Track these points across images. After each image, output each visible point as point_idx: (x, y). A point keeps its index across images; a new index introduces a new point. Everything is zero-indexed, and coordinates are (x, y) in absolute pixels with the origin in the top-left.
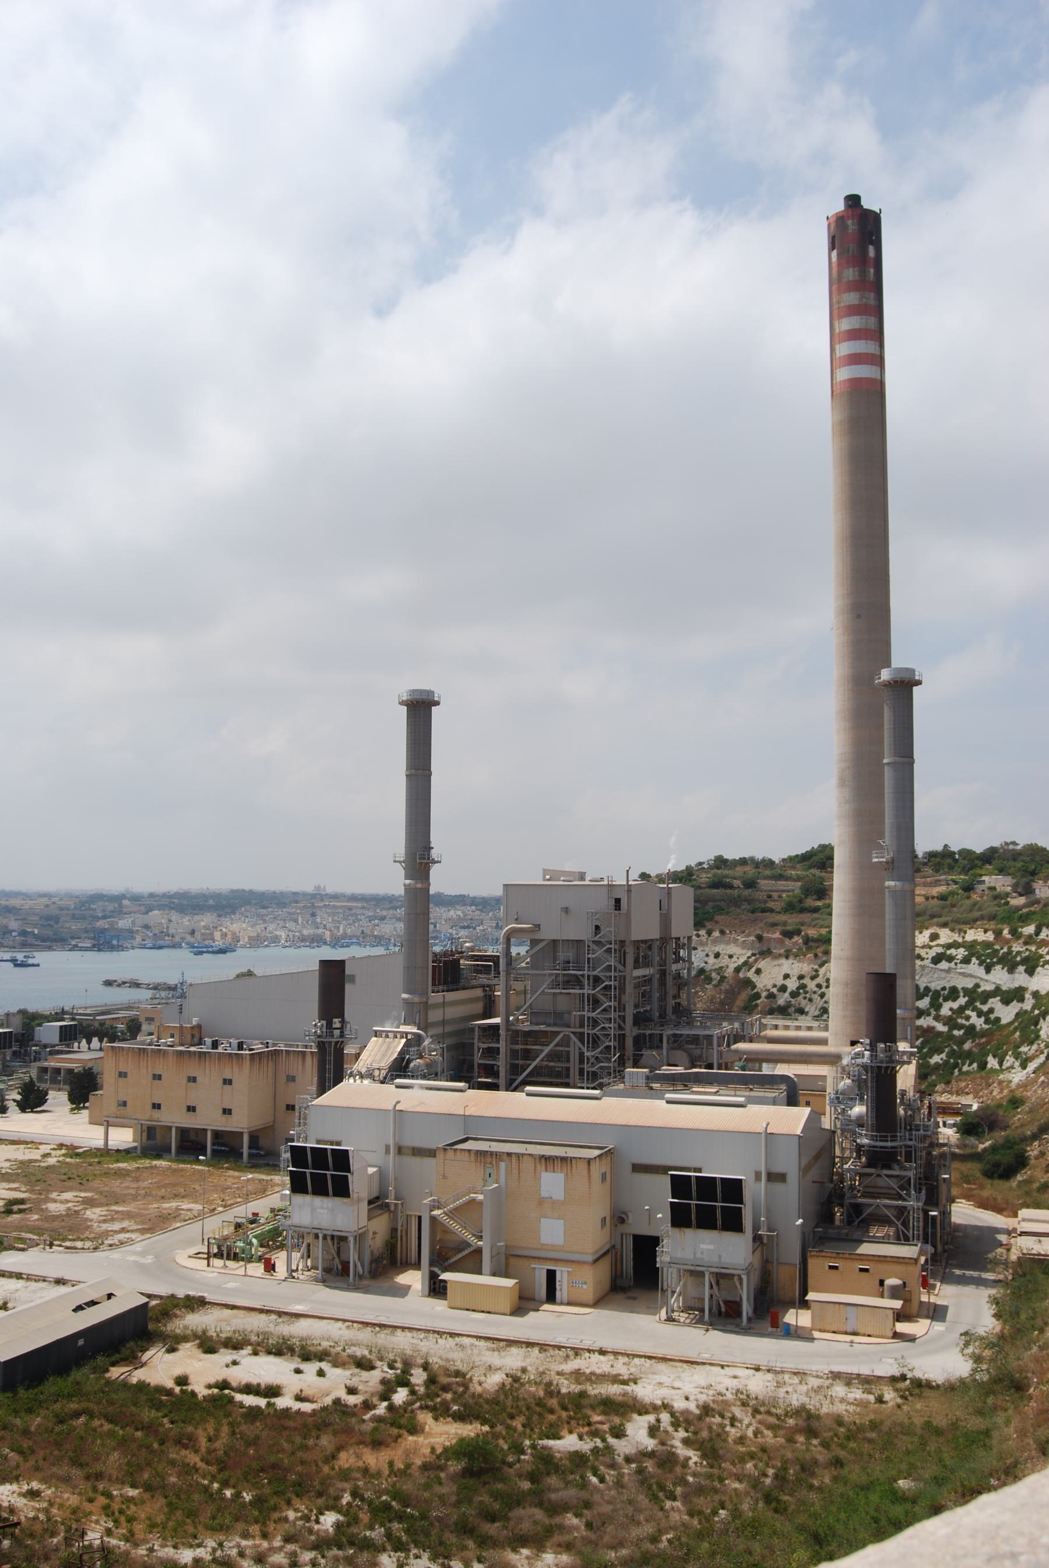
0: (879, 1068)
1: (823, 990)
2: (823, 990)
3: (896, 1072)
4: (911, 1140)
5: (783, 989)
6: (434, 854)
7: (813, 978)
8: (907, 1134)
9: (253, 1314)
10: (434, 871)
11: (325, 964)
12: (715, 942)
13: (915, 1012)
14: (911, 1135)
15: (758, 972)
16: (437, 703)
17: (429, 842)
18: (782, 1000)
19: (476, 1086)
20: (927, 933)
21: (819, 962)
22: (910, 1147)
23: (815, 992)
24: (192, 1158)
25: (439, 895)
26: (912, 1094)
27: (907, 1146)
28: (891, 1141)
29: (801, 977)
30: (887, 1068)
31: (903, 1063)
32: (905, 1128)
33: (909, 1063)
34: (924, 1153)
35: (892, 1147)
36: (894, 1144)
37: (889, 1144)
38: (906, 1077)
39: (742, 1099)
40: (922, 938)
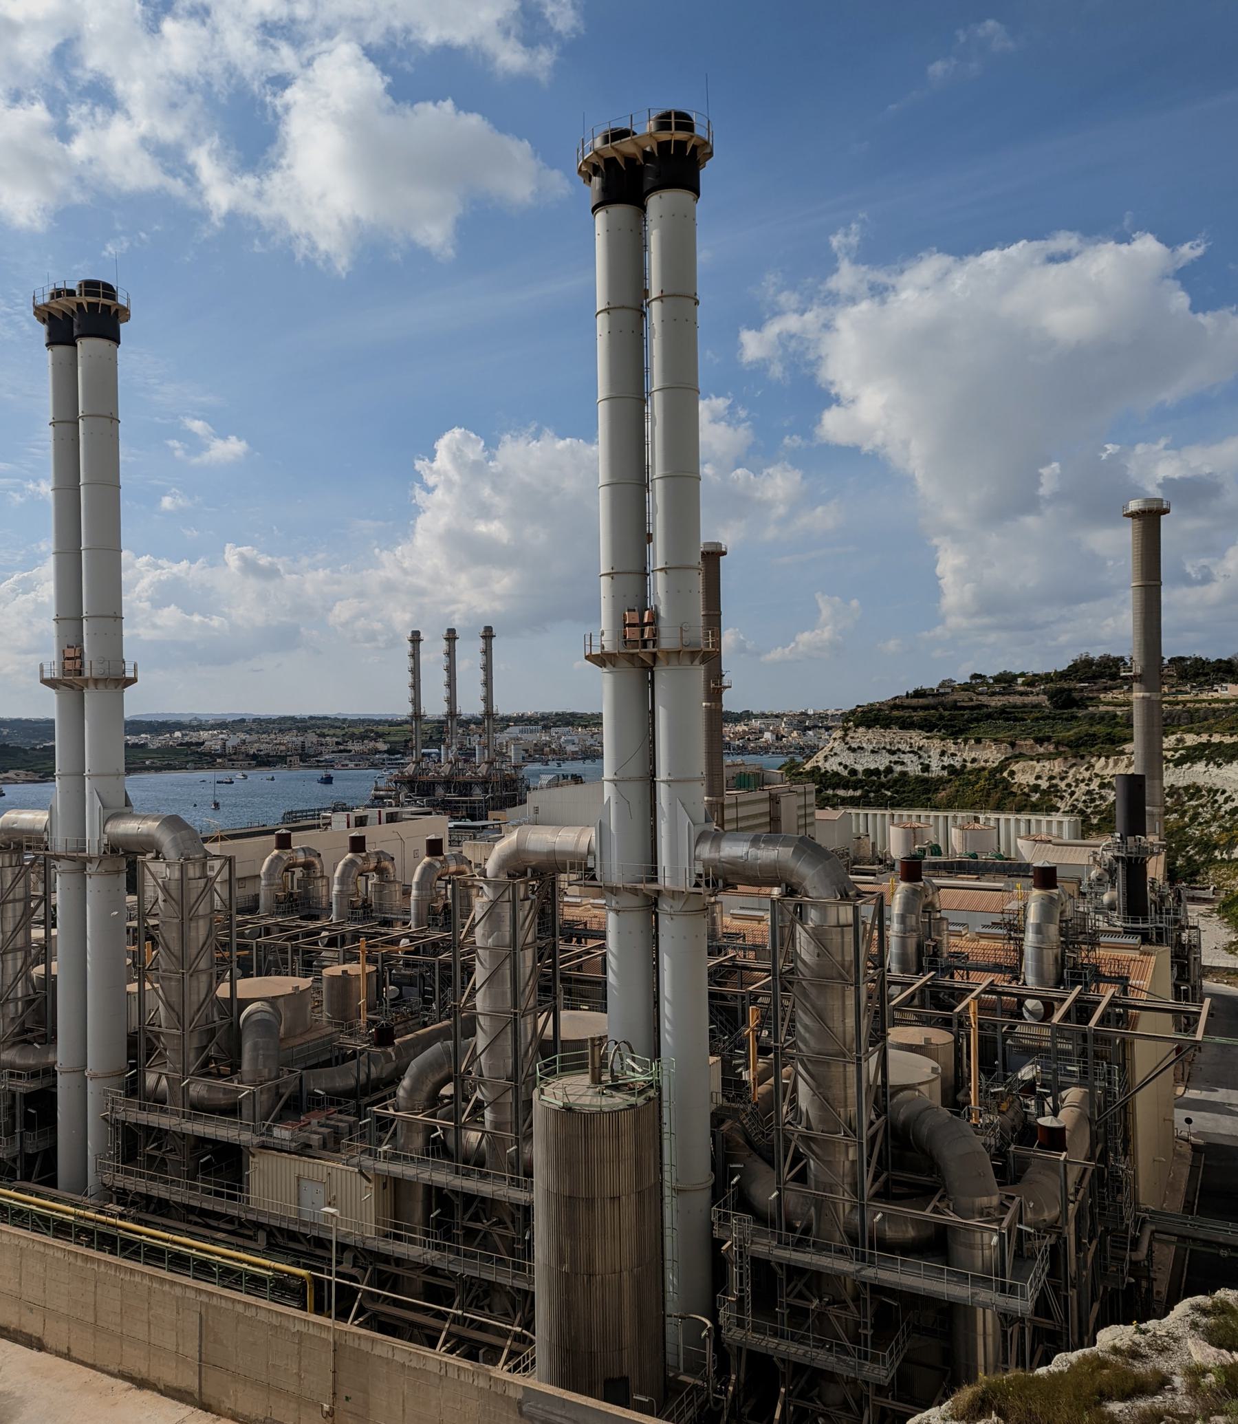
0: (1130, 858)
1: (1073, 789)
2: (1073, 789)
3: (1146, 862)
4: (1161, 922)
5: (1036, 788)
6: (725, 682)
7: (1062, 779)
8: (1158, 917)
9: (148, 1396)
10: (726, 695)
11: (600, 716)
12: (971, 749)
13: (1163, 809)
14: (1161, 918)
15: (1012, 773)
16: (724, 553)
17: (721, 670)
18: (1035, 797)
19: (600, 1388)
20: (1173, 738)
21: (1069, 764)
22: (1161, 928)
23: (1065, 791)
24: (53, 941)
25: (728, 713)
26: (1161, 882)
27: (1157, 928)
28: (50, 922)
29: (1051, 778)
30: (1137, 859)
31: (1153, 854)
32: (1156, 912)
33: (1159, 854)
34: (1174, 935)
35: (1143, 929)
36: (1145, 926)
37: (1141, 925)
38: (1156, 868)
39: (1002, 885)
40: (1170, 741)
